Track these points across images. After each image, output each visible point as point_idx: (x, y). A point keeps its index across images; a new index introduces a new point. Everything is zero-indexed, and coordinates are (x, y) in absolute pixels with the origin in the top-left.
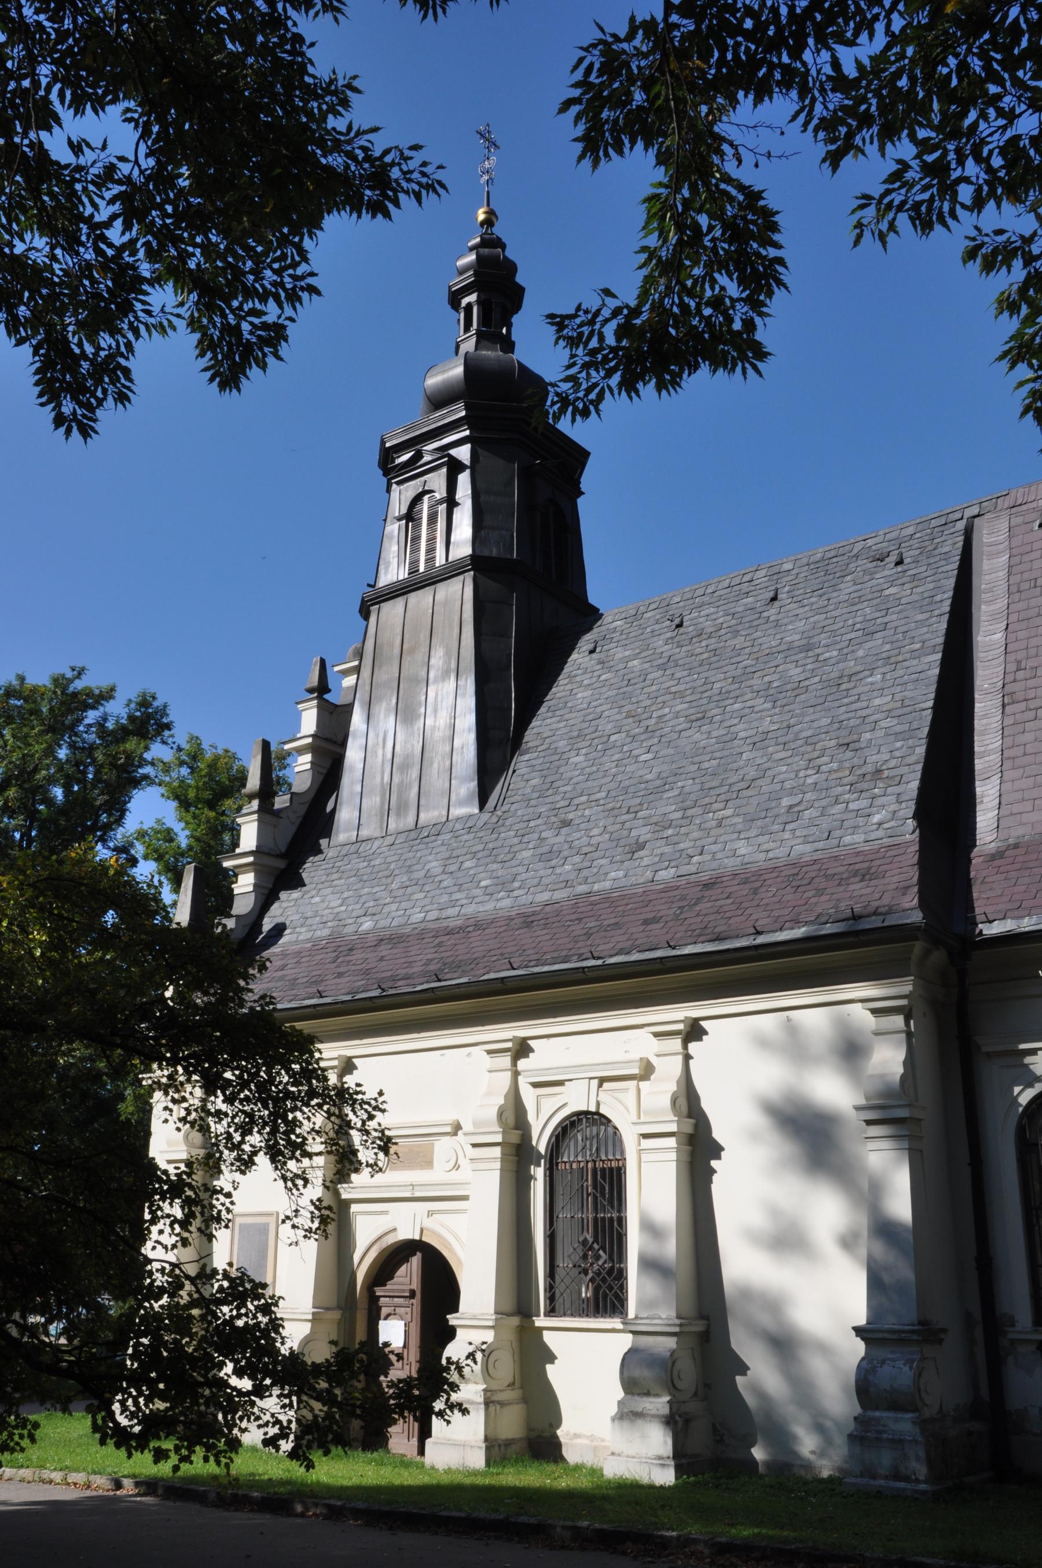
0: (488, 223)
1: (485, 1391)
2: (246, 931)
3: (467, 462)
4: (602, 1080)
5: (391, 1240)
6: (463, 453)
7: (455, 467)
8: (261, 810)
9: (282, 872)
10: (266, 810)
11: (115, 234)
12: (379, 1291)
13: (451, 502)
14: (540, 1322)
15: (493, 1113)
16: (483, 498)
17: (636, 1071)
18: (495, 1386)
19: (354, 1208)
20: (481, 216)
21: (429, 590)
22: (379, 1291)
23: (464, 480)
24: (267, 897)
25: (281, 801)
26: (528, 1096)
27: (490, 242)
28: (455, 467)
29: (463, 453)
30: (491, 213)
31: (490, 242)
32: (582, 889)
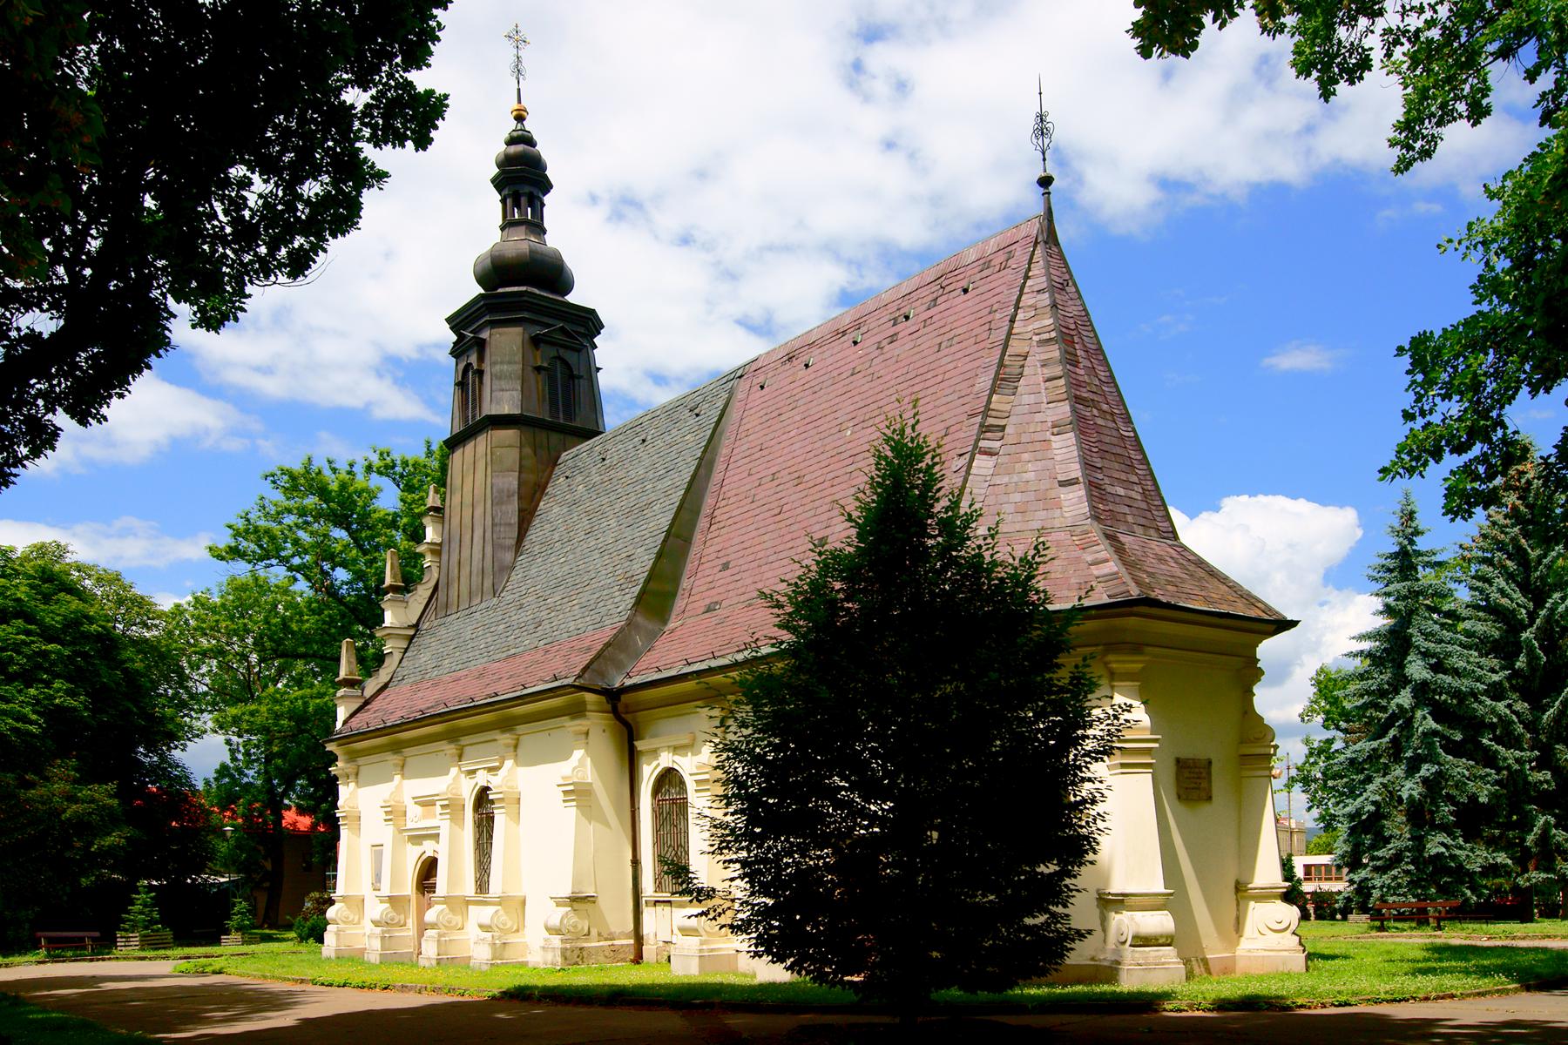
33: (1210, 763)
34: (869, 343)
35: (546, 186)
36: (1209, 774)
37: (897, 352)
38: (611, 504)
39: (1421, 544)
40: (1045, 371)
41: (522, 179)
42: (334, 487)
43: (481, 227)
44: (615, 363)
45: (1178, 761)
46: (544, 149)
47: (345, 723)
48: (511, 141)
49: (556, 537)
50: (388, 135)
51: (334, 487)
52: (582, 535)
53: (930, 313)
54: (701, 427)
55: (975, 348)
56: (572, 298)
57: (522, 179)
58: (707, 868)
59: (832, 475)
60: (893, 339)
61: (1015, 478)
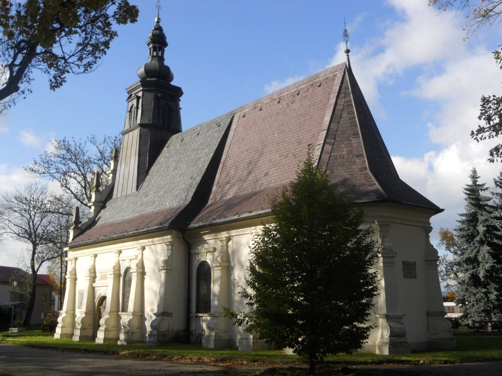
0: (158, 22)
1: (105, 328)
2: (91, 222)
3: (141, 96)
4: (131, 260)
5: (101, 296)
6: (140, 94)
7: (138, 98)
8: (96, 191)
9: (101, 205)
10: (97, 191)
11: (56, 4)
12: (100, 307)
13: (137, 108)
14: (120, 313)
15: (112, 267)
16: (144, 107)
17: (212, 250)
18: (109, 327)
19: (96, 288)
20: (156, 20)
21: (127, 134)
22: (100, 307)
23: (141, 100)
24: (97, 212)
25: (101, 189)
26: (121, 262)
27: (159, 28)
28: (138, 98)
29: (140, 94)
30: (159, 19)
31: (159, 28)
32: (143, 213)
33: (415, 263)
34: (284, 103)
35: (166, 45)
36: (415, 267)
37: (294, 107)
38: (184, 158)
39: (480, 182)
40: (349, 116)
41: (159, 41)
42: (25, 9)
43: (143, 57)
44: (480, 231)
45: (403, 262)
46: (165, 32)
47: (73, 239)
48: (156, 29)
49: (162, 169)
50: (122, 20)
51: (25, 9)
52: (172, 169)
53: (306, 94)
54: (220, 131)
55: (323, 107)
56: (173, 83)
57: (159, 41)
58: (155, 210)
59: (270, 150)
60: (293, 102)
61: (339, 153)
